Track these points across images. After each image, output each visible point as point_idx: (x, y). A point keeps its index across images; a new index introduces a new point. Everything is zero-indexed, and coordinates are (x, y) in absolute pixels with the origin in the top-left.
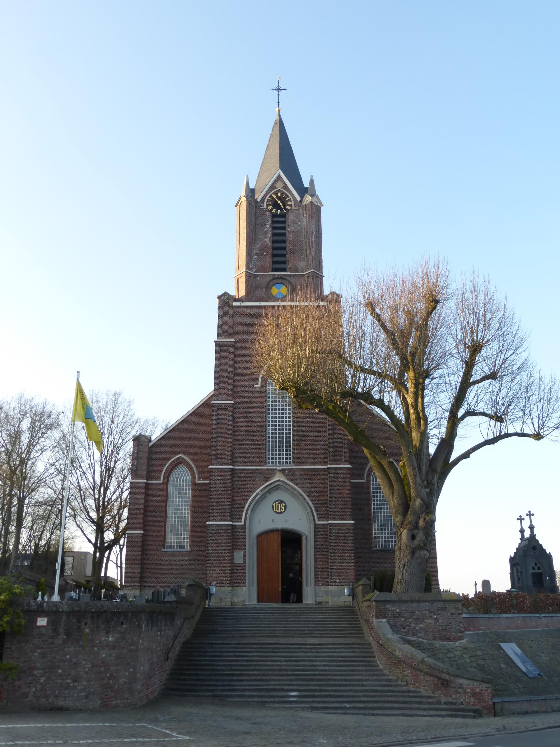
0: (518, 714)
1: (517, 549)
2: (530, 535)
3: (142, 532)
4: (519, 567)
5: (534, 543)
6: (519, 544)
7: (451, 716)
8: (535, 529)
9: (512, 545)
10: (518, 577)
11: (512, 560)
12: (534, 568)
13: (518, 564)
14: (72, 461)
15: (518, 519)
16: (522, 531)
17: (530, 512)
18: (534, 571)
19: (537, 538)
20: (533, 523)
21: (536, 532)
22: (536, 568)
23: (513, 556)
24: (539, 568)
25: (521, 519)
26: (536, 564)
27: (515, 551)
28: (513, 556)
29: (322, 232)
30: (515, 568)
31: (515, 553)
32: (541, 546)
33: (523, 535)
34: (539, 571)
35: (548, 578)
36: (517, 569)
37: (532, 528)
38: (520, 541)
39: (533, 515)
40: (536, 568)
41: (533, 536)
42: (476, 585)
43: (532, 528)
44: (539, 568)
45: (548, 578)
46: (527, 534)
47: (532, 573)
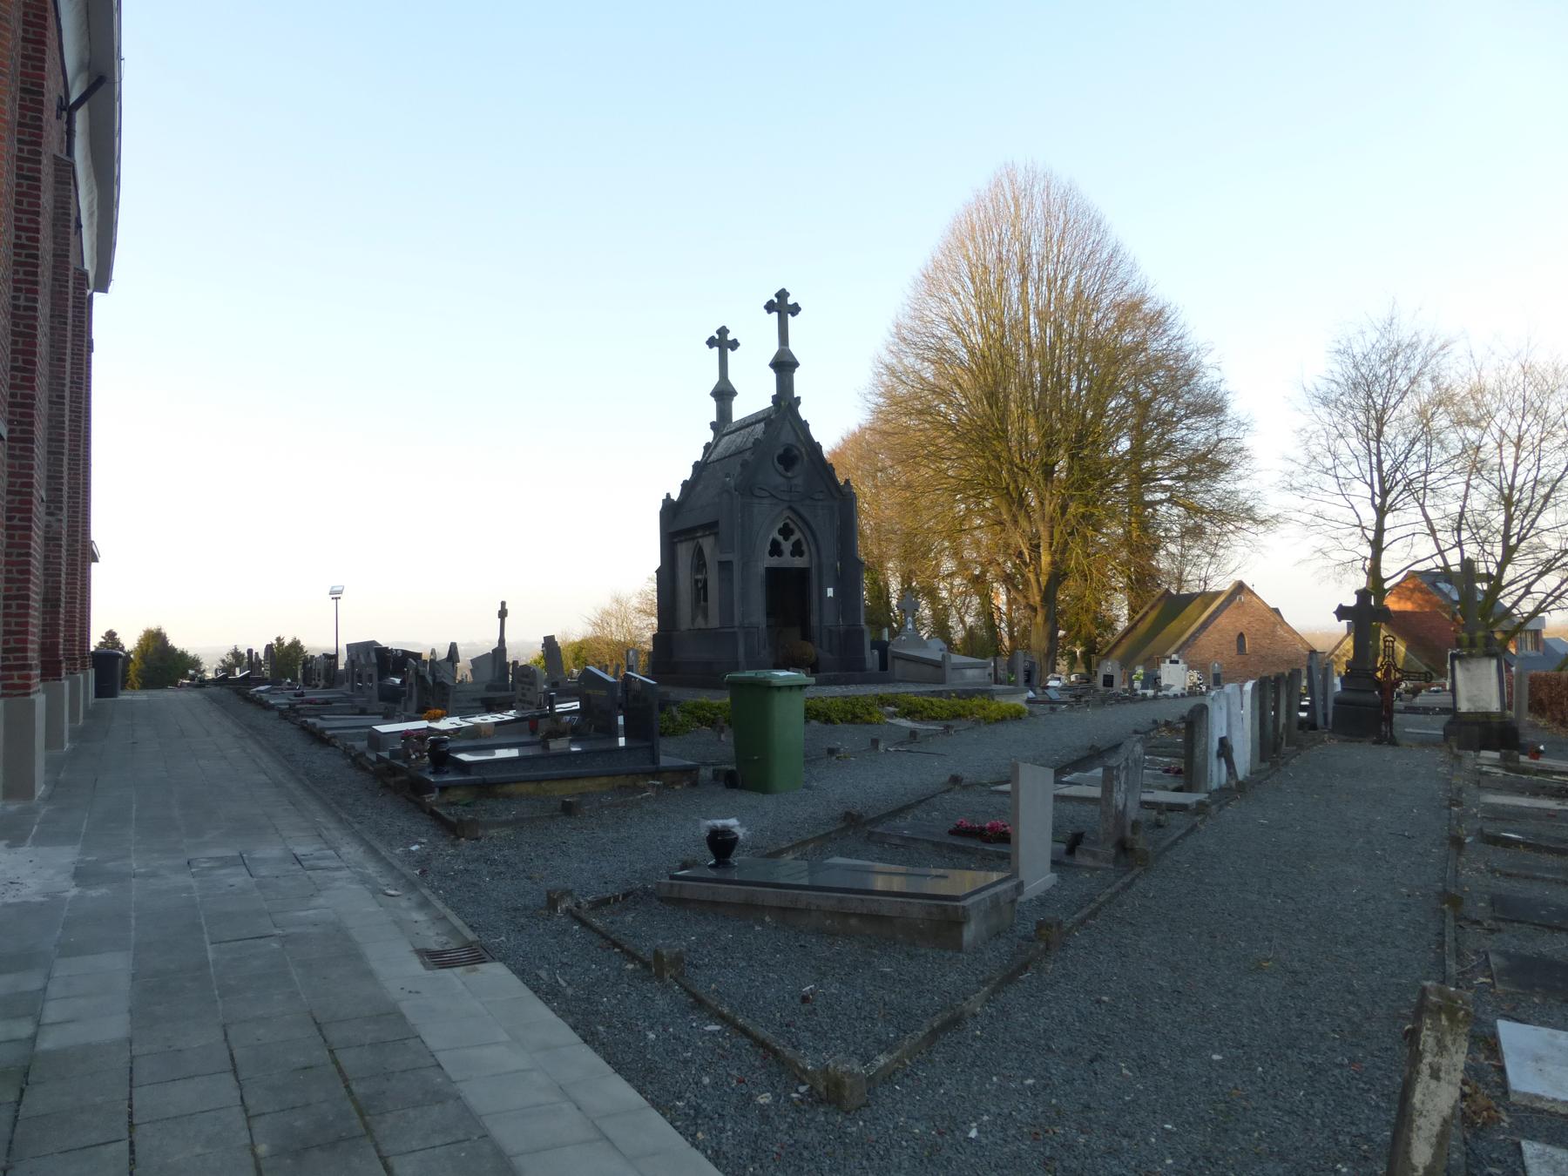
0: (791, 687)
1: (697, 467)
2: (776, 399)
4: (708, 544)
5: (786, 437)
6: (707, 447)
7: (706, 600)
8: (799, 377)
9: (674, 452)
11: (670, 511)
12: (776, 549)
13: (711, 527)
14: (1440, 404)
15: (770, 307)
16: (724, 394)
17: (782, 295)
18: (774, 562)
19: (804, 412)
20: (794, 347)
21: (802, 384)
22: (787, 546)
23: (675, 496)
24: (797, 550)
25: (722, 342)
26: (786, 532)
27: (687, 474)
28: (675, 496)
30: (684, 552)
31: (685, 485)
34: (798, 562)
35: (830, 592)
37: (784, 365)
38: (709, 436)
39: (795, 310)
40: (787, 546)
41: (785, 402)
42: (503, 614)
43: (784, 365)
44: (797, 550)
45: (830, 592)
47: (769, 570)
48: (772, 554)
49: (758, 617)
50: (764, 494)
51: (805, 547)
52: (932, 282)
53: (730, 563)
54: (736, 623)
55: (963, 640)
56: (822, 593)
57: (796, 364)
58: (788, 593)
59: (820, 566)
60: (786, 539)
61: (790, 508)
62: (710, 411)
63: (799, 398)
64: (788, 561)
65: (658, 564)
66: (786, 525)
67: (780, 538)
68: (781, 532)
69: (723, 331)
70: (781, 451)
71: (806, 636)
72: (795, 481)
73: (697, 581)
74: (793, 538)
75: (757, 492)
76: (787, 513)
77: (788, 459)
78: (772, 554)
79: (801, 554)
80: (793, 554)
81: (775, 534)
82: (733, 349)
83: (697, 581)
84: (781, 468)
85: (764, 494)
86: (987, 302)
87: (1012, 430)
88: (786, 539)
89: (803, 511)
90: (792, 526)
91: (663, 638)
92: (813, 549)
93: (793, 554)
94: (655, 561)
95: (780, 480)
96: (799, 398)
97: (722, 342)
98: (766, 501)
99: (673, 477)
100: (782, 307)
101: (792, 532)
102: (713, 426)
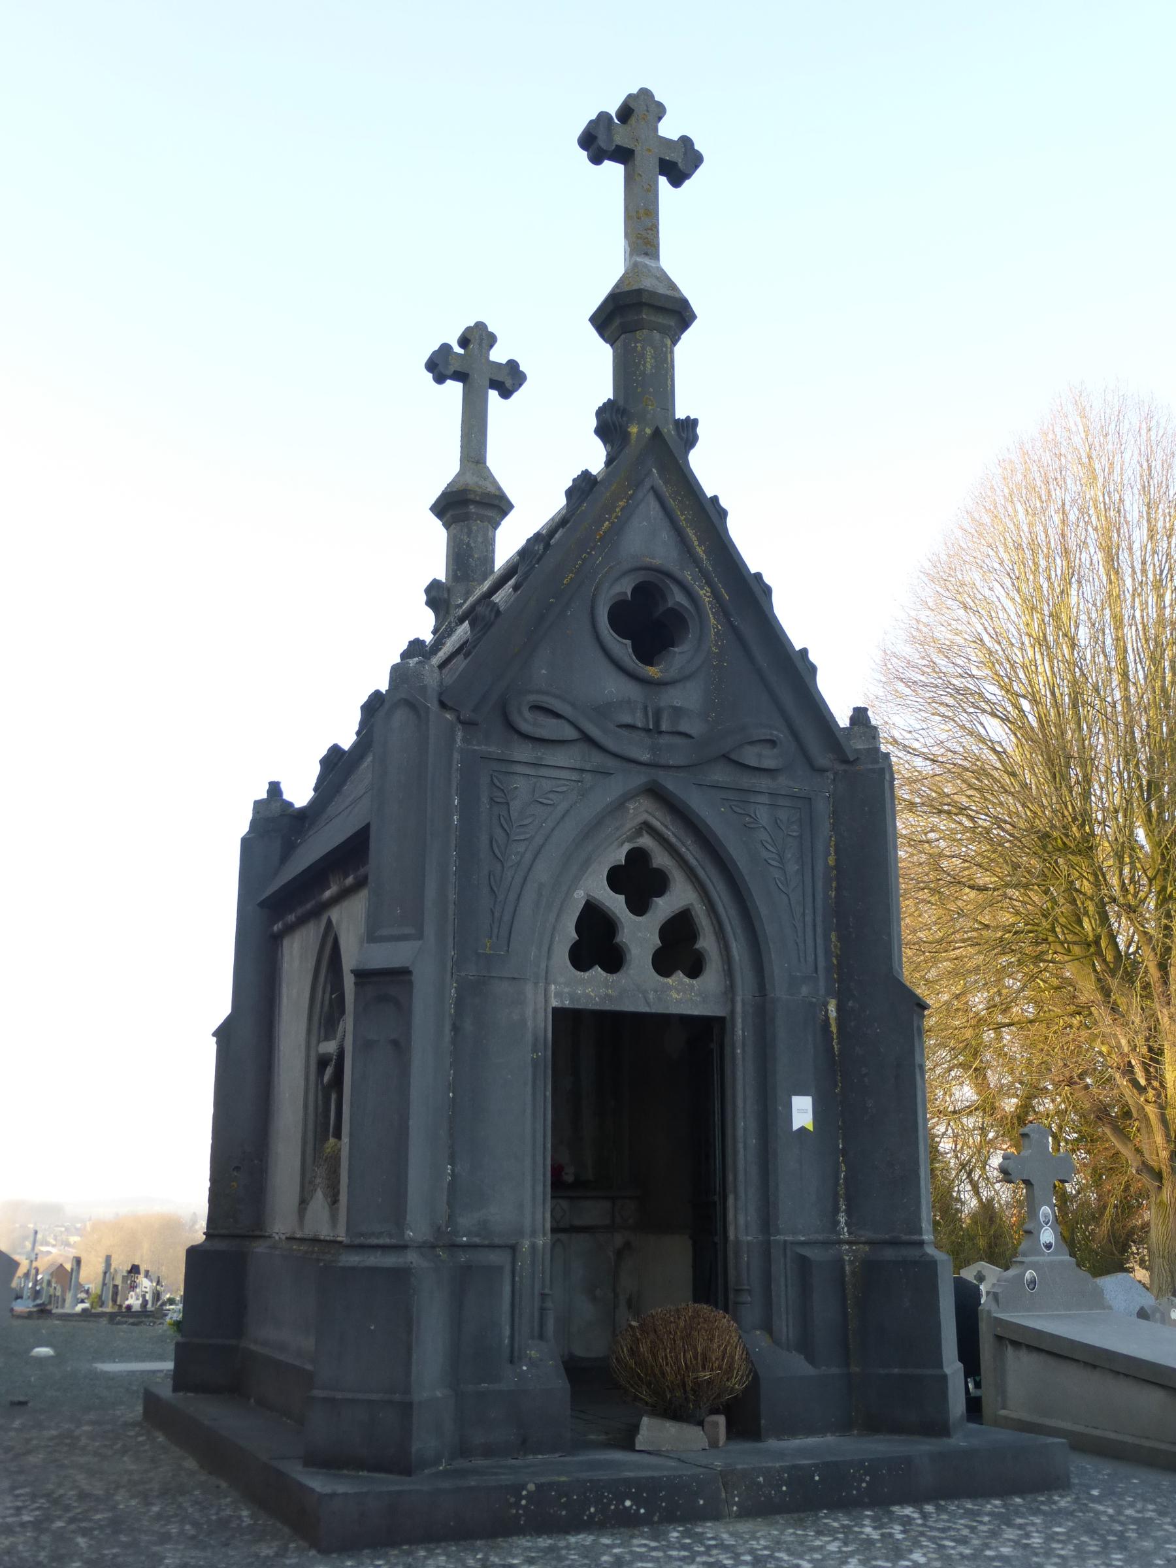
1: (374, 707)
3: (834, 1370)
5: (647, 541)
8: (691, 356)
9: (322, 635)
10: (328, 1076)
12: (597, 944)
15: (440, 366)
16: (469, 505)
18: (593, 989)
19: (707, 466)
21: (699, 376)
22: (640, 935)
23: (300, 794)
24: (678, 950)
25: (473, 368)
26: (637, 880)
28: (300, 794)
29: (207, 1184)
30: (298, 956)
32: (748, 596)
33: (467, 557)
34: (682, 996)
35: (802, 1112)
36: (330, 957)
40: (640, 935)
41: (644, 435)
44: (678, 950)
45: (802, 1112)
46: (546, 453)
47: (568, 1021)
48: (581, 958)
49: (518, 1201)
50: (548, 727)
51: (707, 943)
52: (949, 582)
53: (400, 975)
54: (417, 1230)
55: (974, 1217)
56: (771, 1114)
57: (695, 422)
58: (641, 1112)
59: (763, 1012)
60: (639, 906)
61: (655, 792)
62: (429, 552)
63: (690, 425)
64: (640, 987)
65: (222, 1008)
66: (638, 857)
67: (616, 903)
68: (616, 879)
69: (477, 338)
70: (625, 587)
71: (711, 1283)
72: (676, 697)
73: (323, 1062)
74: (664, 907)
75: (527, 722)
76: (643, 810)
77: (648, 622)
78: (581, 958)
79: (695, 969)
80: (664, 963)
81: (595, 886)
82: (506, 393)
83: (323, 1062)
84: (623, 649)
85: (548, 727)
86: (1053, 628)
87: (1105, 834)
88: (639, 906)
89: (698, 803)
90: (661, 859)
91: (223, 1261)
92: (738, 949)
93: (664, 963)
94: (215, 998)
95: (614, 687)
96: (690, 425)
97: (473, 368)
98: (559, 757)
99: (295, 724)
100: (635, 145)
101: (658, 884)
102: (436, 596)
